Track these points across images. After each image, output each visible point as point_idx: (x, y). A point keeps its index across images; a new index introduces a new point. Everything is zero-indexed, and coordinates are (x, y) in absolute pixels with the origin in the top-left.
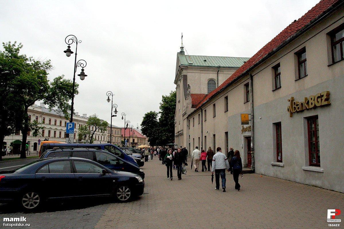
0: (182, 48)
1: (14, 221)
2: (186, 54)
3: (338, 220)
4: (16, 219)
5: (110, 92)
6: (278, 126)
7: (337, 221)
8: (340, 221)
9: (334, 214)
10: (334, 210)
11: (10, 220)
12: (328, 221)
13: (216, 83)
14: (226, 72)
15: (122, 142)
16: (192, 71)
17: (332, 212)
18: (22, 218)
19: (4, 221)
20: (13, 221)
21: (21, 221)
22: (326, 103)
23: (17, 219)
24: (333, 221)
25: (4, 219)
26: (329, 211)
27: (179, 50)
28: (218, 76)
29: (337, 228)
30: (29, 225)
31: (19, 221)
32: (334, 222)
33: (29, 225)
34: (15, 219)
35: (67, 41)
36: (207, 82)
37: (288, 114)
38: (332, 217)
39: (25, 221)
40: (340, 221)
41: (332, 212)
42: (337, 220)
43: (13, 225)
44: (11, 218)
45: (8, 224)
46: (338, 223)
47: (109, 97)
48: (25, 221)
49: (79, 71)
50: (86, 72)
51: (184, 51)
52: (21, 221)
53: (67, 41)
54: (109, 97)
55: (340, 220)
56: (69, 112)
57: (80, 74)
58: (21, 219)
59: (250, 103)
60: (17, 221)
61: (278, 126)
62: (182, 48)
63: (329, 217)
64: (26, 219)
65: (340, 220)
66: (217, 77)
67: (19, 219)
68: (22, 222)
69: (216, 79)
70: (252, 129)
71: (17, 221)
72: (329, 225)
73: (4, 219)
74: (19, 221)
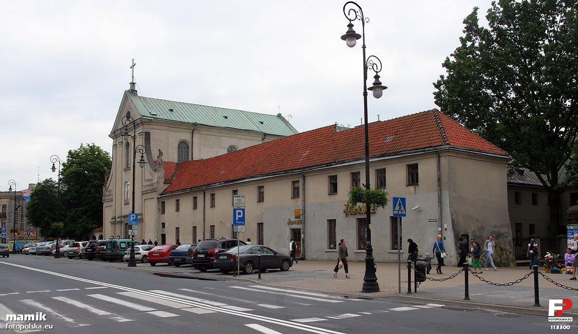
0: (133, 84)
1: (26, 319)
2: (139, 94)
3: (567, 318)
4: (28, 317)
5: (55, 157)
6: (332, 223)
7: (566, 321)
8: (572, 321)
9: (560, 308)
10: (560, 301)
11: (18, 319)
12: (550, 321)
13: (190, 147)
14: (204, 132)
15: (131, 227)
16: (157, 127)
17: (556, 305)
18: (39, 314)
19: (7, 319)
20: (22, 319)
21: (37, 319)
22: (373, 211)
23: (29, 316)
24: (558, 321)
25: (8, 316)
26: (552, 303)
27: (128, 88)
28: (192, 137)
29: (562, 333)
30: (51, 327)
31: (33, 319)
32: (560, 321)
33: (51, 327)
34: (26, 316)
35: (52, 159)
36: (177, 145)
37: (344, 215)
38: (558, 313)
39: (44, 319)
40: (572, 321)
41: (556, 305)
42: (565, 318)
43: (22, 327)
44: (19, 315)
45: (14, 325)
46: (567, 323)
47: (54, 165)
48: (44, 319)
49: (370, 82)
50: (383, 81)
51: (136, 89)
52: (37, 319)
53: (52, 159)
54: (54, 165)
55: (572, 318)
56: (117, 133)
57: (372, 86)
58: (37, 316)
59: (300, 199)
60: (29, 319)
61: (332, 223)
62: (133, 84)
63: (551, 313)
64: (45, 317)
65: (572, 318)
66: (191, 138)
67: (33, 316)
68: (38, 322)
69: (191, 142)
70: (303, 222)
71: (29, 319)
72: (552, 326)
73: (8, 316)
74: (33, 319)
